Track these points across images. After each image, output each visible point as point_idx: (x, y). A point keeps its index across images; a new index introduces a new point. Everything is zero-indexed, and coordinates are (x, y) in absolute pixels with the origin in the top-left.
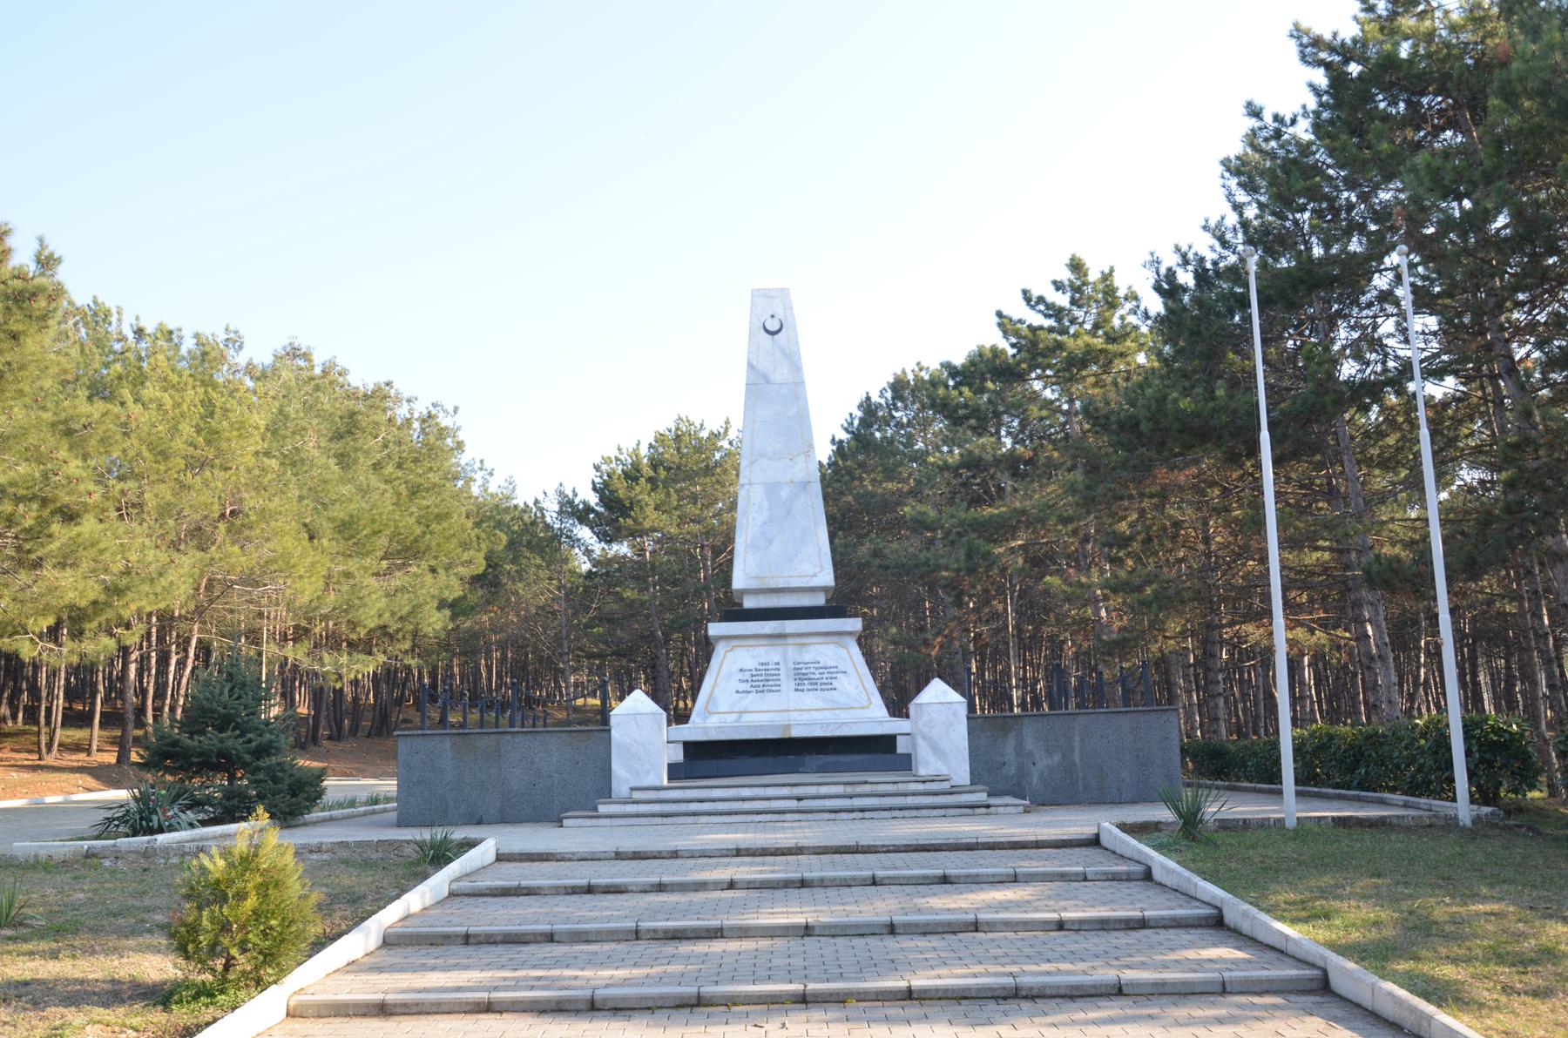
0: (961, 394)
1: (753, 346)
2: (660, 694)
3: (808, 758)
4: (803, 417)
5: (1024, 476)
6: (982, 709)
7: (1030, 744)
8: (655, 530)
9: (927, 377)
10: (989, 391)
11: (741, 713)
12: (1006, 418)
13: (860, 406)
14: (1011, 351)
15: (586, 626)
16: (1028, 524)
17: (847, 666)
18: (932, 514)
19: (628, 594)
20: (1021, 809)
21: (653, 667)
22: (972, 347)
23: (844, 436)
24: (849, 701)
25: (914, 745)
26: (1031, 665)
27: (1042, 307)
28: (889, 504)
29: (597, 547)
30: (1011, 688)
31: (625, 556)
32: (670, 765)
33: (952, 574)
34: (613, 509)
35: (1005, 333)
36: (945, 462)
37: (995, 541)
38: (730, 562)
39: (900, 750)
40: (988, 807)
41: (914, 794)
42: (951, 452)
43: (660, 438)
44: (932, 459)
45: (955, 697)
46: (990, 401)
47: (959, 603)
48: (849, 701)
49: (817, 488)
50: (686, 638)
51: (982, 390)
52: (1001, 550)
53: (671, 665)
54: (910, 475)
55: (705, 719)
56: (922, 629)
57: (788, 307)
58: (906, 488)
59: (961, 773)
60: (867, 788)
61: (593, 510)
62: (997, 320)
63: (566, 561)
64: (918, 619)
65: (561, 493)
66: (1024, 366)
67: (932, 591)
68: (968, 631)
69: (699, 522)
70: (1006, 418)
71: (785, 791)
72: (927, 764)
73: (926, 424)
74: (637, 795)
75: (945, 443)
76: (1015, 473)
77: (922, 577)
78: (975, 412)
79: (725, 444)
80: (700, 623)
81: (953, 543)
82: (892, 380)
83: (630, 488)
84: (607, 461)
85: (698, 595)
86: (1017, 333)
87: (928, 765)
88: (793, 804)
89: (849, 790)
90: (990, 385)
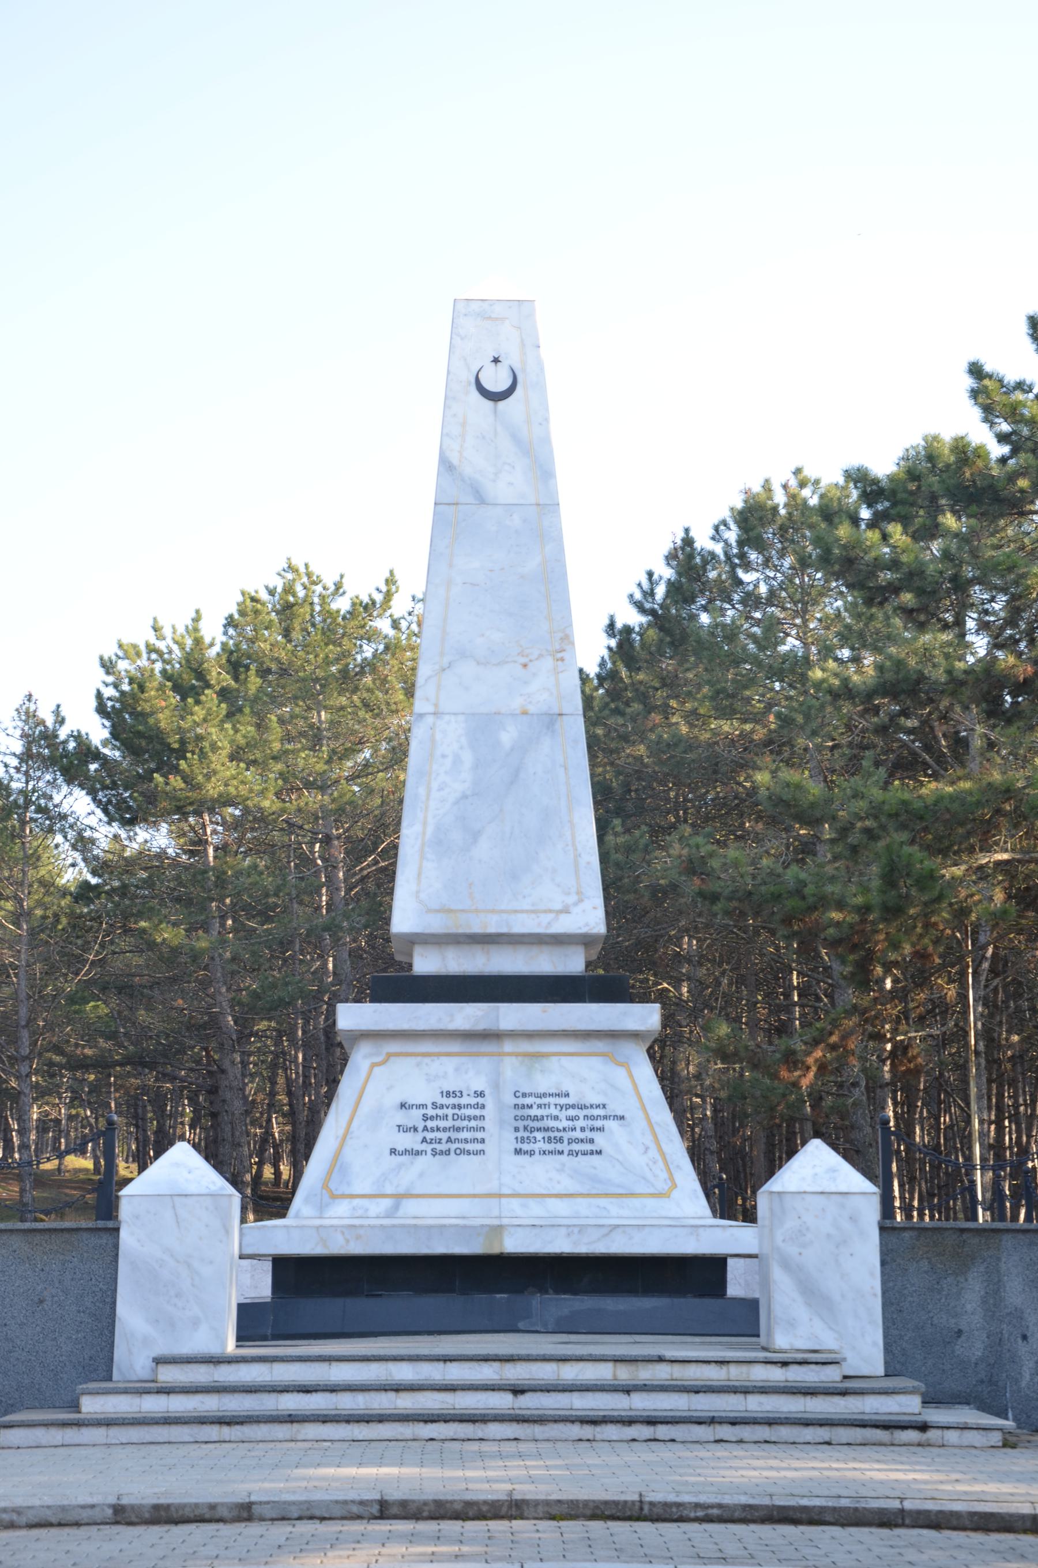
0: (885, 537)
1: (453, 428)
2: (225, 1150)
3: (536, 1301)
4: (552, 580)
5: (1010, 717)
6: (907, 1209)
7: (1015, 1292)
8: (228, 801)
9: (814, 501)
10: (946, 533)
11: (399, 1197)
12: (978, 593)
13: (671, 557)
14: (997, 450)
15: (72, 1000)
16: (1018, 818)
18: (815, 789)
19: (168, 935)
20: (996, 1438)
21: (213, 1091)
22: (914, 439)
23: (634, 619)
25: (765, 1282)
26: (1015, 1118)
28: (721, 765)
29: (105, 834)
30: (971, 1168)
31: (162, 855)
32: (242, 1308)
33: (853, 918)
34: (139, 753)
35: (989, 412)
36: (846, 681)
37: (944, 852)
38: (387, 877)
39: (734, 1290)
40: (924, 1427)
41: (764, 1390)
42: (856, 660)
43: (250, 607)
44: (818, 674)
45: (851, 1179)
46: (946, 555)
47: (863, 979)
48: (644, 1192)
49: (576, 728)
50: (284, 1032)
51: (931, 531)
52: (958, 871)
53: (251, 1088)
54: (769, 707)
55: (322, 1208)
56: (783, 1029)
57: (530, 343)
58: (760, 734)
59: (865, 1350)
60: (661, 1373)
61: (97, 756)
62: (969, 382)
63: (33, 859)
64: (776, 1010)
65: (29, 716)
66: (1023, 483)
67: (807, 951)
68: (880, 1037)
69: (322, 789)
70: (978, 593)
71: (487, 1372)
72: (792, 1324)
73: (806, 601)
74: (168, 1375)
75: (845, 639)
76: (994, 712)
77: (787, 921)
78: (913, 577)
79: (383, 625)
80: (322, 1002)
81: (854, 850)
82: (739, 505)
83: (184, 711)
84: (129, 651)
85: (313, 940)
86: (1013, 413)
87: (793, 1325)
88: (502, 1402)
89: (625, 1374)
90: (949, 520)
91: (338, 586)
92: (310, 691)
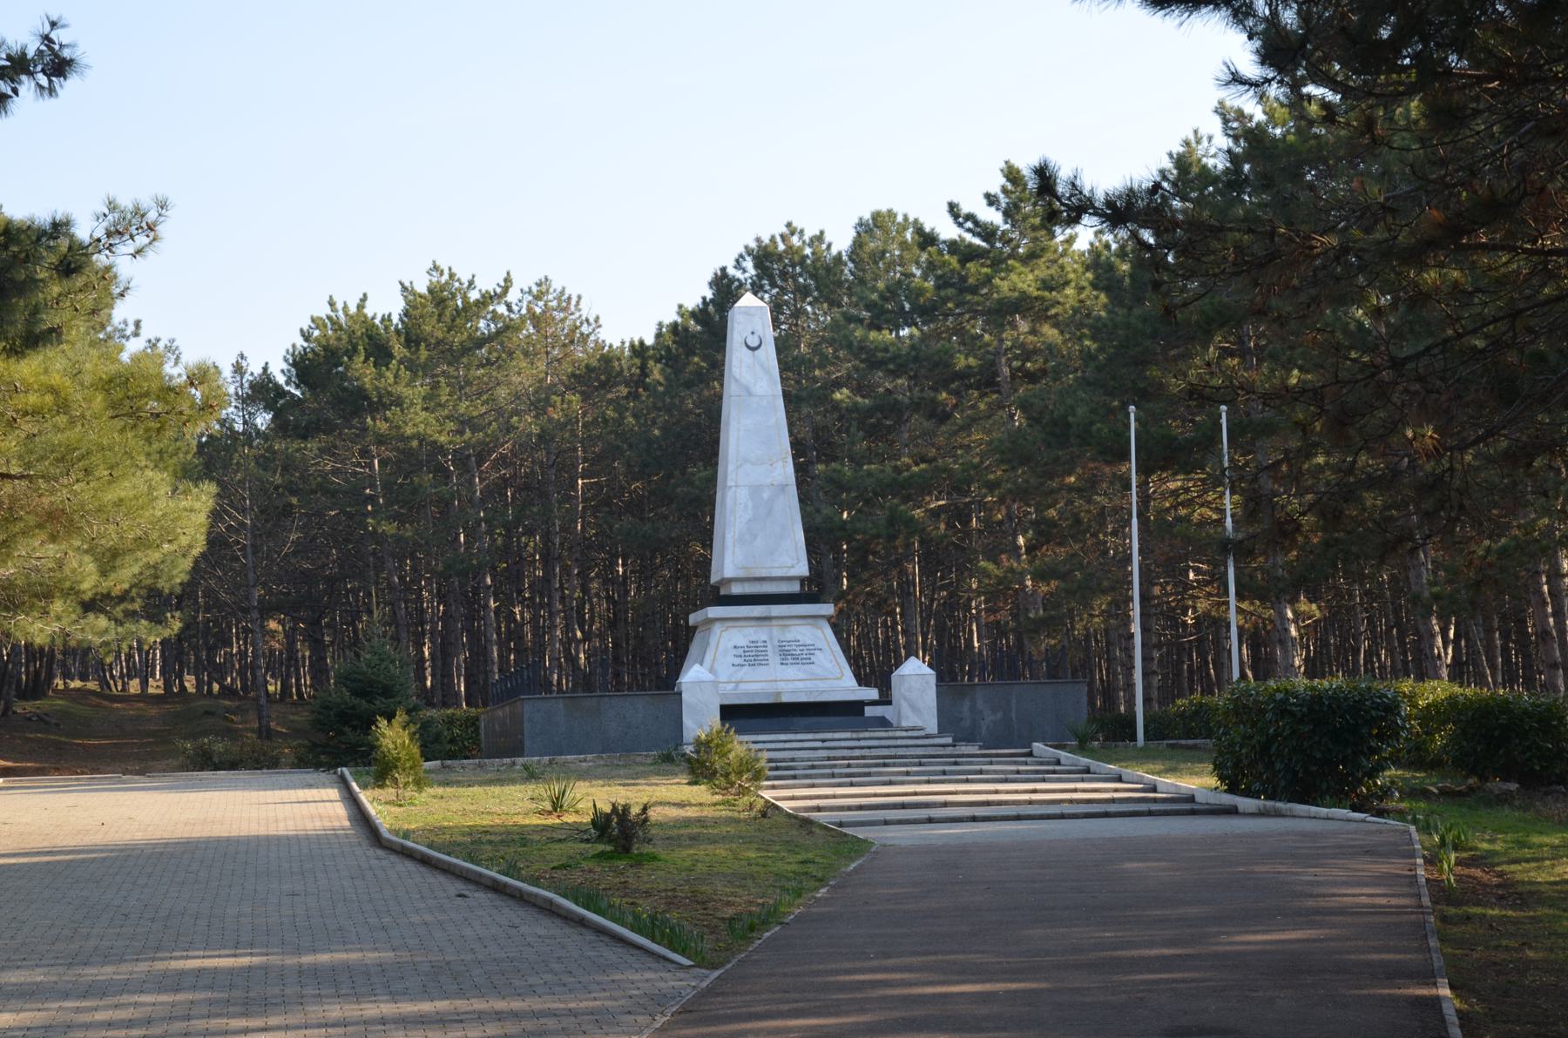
3: (796, 720)
7: (980, 704)
17: (825, 647)
24: (828, 674)
27: (969, 225)
48: (828, 674)
88: (819, 744)
91: (471, 283)
92: (454, 355)
